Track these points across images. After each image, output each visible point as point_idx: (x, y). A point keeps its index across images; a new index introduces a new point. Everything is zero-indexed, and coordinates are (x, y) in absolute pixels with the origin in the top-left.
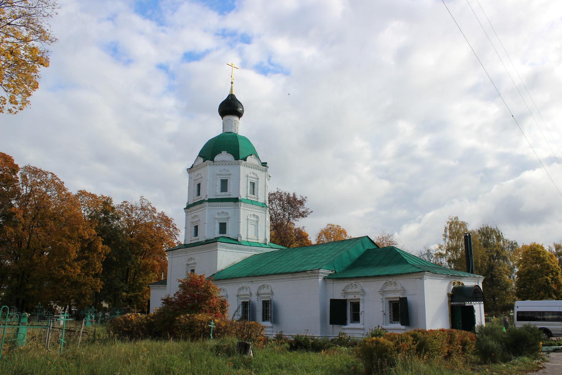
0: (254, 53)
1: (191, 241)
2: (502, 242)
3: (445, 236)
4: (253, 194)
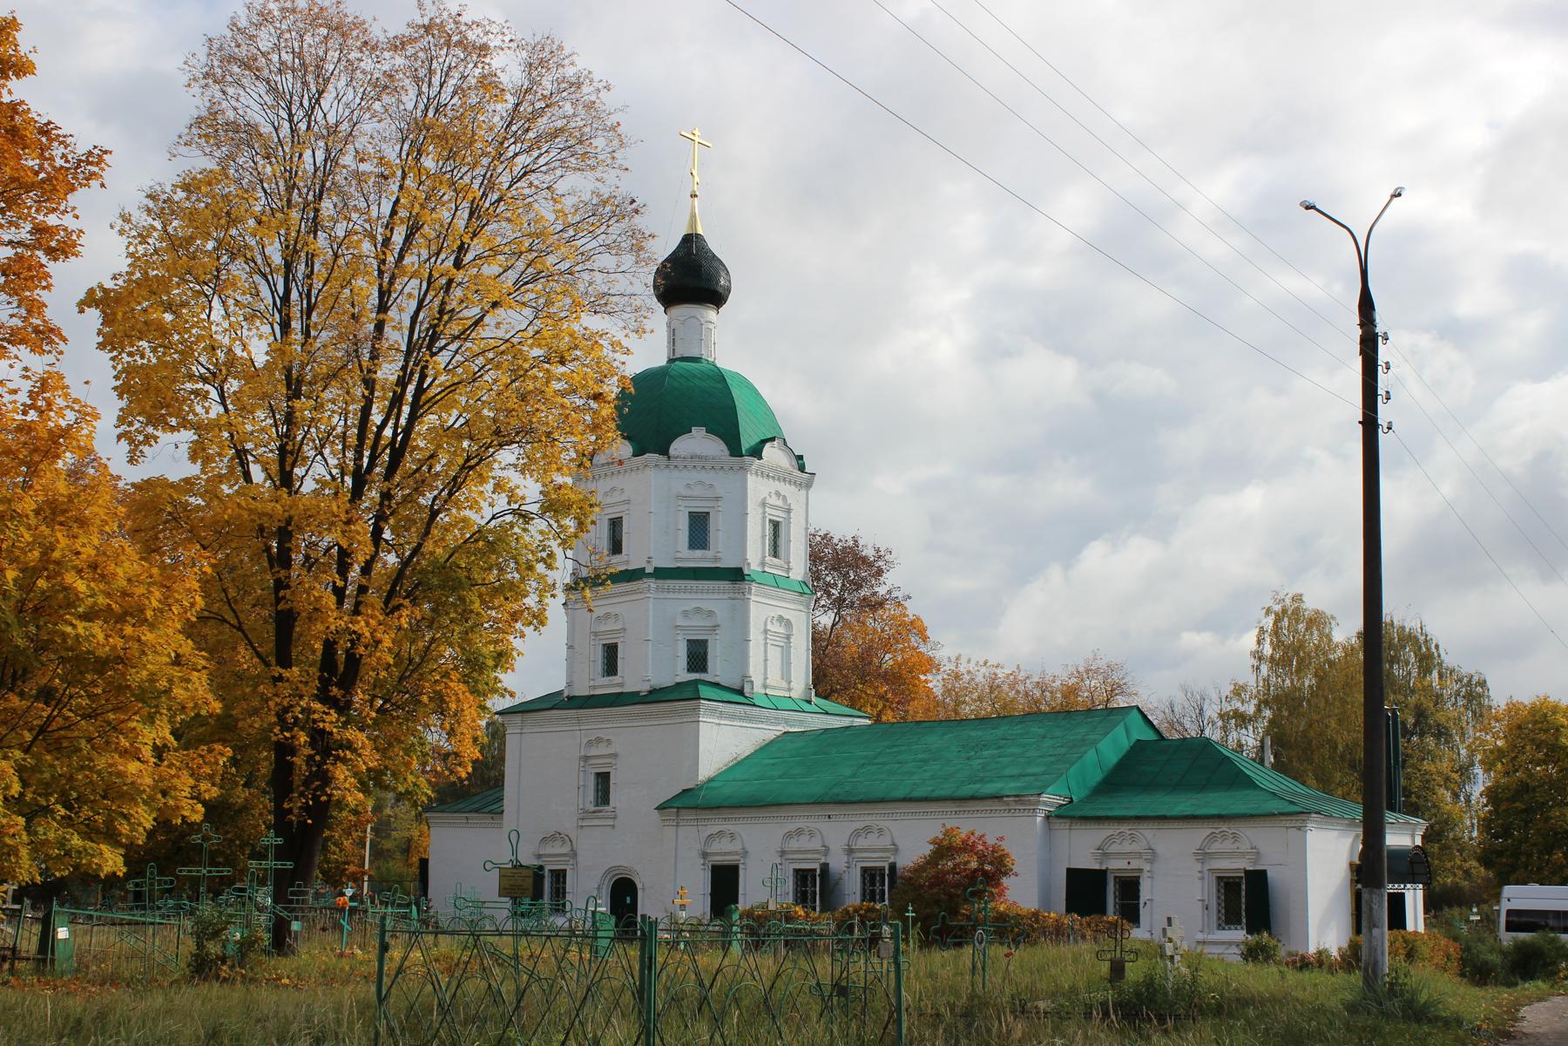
2: (1435, 674)
3: (1258, 656)
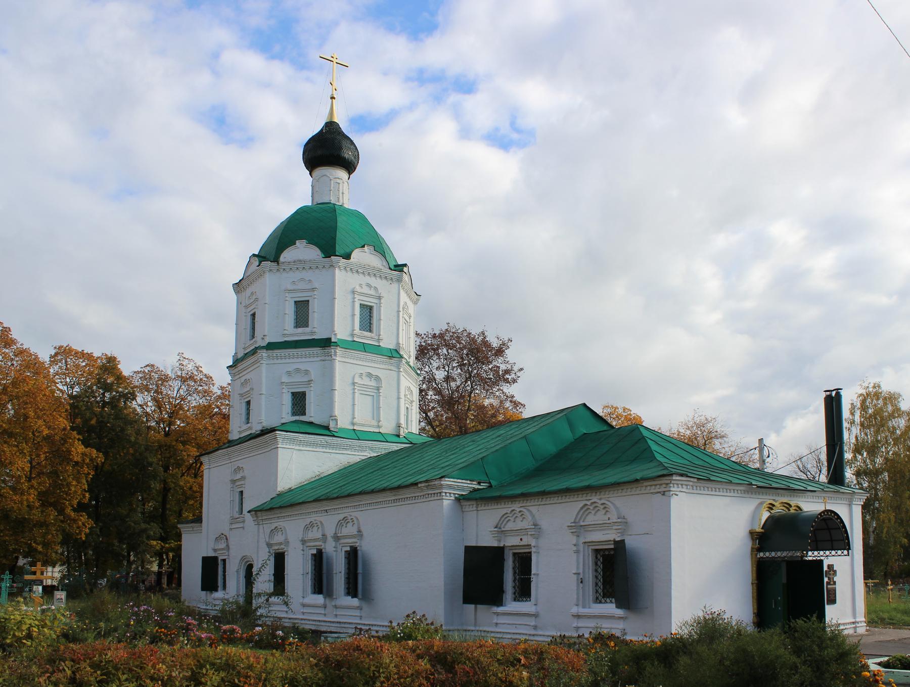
0: (481, 109)
1: (240, 432)
4: (370, 331)
